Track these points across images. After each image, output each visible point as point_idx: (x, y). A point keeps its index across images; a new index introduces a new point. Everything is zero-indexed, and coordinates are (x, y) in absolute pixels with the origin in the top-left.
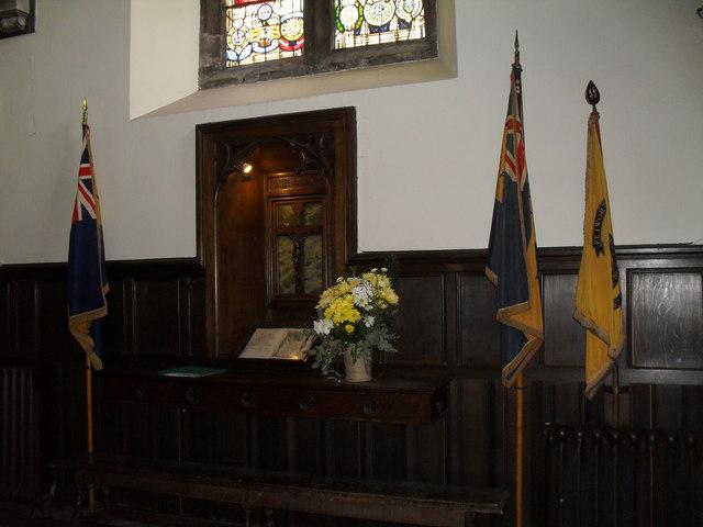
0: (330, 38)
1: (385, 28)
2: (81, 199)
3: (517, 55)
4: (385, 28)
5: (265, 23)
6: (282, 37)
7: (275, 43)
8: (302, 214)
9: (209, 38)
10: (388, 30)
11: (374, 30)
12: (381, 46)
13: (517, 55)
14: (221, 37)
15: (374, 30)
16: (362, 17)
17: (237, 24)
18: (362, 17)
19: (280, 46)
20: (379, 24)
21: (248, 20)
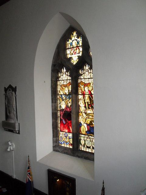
0: (78, 147)
1: (89, 148)
2: (28, 177)
3: (103, 186)
4: (89, 148)
5: (66, 137)
6: (69, 142)
7: (68, 143)
8: (81, 95)
9: (55, 139)
10: (90, 148)
11: (88, 147)
12: (86, 152)
13: (103, 186)
14: (57, 138)
15: (88, 147)
16: (85, 143)
17: (61, 135)
18: (85, 143)
19: (69, 144)
20: (88, 146)
21: (63, 135)
